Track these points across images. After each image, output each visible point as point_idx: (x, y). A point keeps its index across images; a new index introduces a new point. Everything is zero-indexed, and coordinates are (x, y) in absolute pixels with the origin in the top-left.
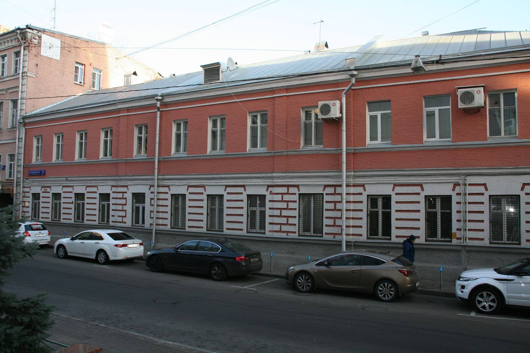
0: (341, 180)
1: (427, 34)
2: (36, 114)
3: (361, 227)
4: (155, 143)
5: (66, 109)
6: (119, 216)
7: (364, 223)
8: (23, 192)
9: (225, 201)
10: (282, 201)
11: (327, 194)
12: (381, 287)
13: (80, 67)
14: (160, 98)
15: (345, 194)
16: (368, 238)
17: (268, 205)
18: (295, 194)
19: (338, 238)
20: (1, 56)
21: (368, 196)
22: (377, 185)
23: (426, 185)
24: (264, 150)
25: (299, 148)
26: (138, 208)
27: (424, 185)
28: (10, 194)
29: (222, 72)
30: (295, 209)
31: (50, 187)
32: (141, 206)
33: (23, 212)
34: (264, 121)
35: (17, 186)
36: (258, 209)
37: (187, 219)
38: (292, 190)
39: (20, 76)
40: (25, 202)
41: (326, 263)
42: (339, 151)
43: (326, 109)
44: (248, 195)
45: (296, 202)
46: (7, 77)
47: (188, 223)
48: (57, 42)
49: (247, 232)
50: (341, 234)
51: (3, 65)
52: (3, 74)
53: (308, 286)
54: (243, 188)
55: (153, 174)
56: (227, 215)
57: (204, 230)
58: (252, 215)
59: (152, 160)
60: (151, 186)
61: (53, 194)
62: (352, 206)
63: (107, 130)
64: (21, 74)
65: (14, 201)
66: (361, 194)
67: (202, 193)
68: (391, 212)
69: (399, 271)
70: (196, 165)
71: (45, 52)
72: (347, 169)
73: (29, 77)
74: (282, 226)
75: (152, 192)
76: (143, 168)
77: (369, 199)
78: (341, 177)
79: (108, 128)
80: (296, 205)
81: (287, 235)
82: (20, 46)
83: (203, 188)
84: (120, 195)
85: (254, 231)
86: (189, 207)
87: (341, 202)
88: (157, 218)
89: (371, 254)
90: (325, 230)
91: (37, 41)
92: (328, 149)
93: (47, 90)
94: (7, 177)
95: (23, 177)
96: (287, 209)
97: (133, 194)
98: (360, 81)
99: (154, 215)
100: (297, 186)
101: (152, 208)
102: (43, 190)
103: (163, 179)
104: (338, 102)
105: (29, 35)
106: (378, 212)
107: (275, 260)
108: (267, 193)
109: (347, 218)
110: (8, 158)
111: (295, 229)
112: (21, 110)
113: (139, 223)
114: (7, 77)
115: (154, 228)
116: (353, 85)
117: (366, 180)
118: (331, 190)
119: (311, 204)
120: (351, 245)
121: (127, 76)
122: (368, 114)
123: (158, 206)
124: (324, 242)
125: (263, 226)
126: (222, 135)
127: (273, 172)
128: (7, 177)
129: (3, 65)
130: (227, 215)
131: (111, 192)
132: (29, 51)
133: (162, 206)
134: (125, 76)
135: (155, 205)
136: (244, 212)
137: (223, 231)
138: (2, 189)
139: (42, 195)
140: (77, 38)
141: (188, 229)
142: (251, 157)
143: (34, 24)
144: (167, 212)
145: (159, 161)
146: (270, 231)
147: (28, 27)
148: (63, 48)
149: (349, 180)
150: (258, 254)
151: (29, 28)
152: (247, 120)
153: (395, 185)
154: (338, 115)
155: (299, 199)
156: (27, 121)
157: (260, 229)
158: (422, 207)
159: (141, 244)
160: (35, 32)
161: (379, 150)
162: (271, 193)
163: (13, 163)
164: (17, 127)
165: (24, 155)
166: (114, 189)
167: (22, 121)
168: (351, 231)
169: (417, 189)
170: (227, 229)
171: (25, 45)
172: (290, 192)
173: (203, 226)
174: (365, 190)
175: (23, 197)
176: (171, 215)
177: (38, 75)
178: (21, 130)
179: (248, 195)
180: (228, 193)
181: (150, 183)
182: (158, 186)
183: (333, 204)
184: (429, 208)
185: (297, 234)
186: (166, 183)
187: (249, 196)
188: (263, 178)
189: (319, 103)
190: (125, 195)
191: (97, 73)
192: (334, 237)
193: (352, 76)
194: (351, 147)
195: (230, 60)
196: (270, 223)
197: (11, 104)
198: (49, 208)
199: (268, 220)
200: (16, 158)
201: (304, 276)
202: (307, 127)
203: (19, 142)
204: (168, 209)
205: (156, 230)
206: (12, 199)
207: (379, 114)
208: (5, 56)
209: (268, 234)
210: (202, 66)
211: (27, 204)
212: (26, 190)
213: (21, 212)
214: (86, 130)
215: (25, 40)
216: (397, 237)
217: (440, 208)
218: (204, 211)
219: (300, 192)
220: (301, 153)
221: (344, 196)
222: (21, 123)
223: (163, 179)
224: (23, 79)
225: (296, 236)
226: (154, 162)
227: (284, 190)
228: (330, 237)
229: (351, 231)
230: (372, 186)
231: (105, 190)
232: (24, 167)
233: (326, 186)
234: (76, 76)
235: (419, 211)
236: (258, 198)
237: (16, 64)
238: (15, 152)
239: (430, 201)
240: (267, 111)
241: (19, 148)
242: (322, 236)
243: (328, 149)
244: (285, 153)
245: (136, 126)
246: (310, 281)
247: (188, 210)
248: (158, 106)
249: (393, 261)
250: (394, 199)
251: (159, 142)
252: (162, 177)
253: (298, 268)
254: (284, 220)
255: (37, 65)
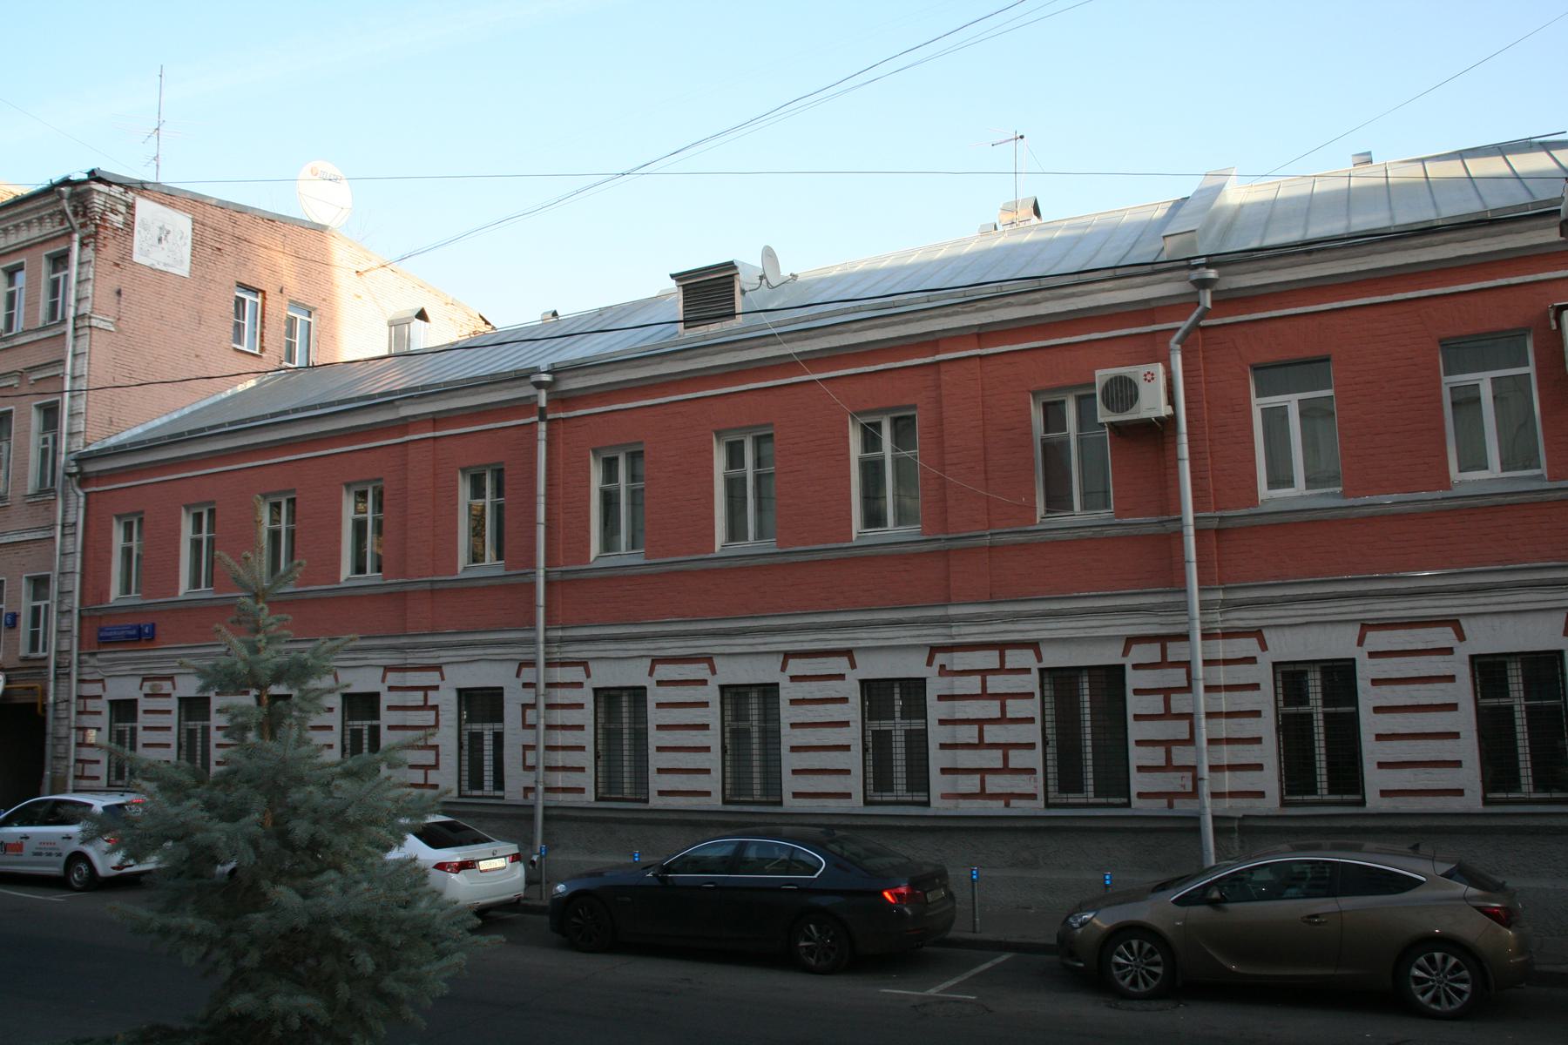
0: (1185, 619)
1: (1366, 159)
2: (124, 446)
3: (1259, 767)
4: (533, 523)
5: (222, 425)
6: (412, 767)
7: (1268, 753)
8: (79, 697)
9: (784, 705)
10: (984, 695)
11: (1136, 667)
12: (1420, 968)
13: (249, 298)
14: (546, 378)
15: (1200, 663)
16: (1284, 804)
17: (936, 710)
18: (1027, 671)
19: (1183, 807)
20: (4, 270)
21: (1275, 664)
22: (1306, 628)
23: (1472, 621)
24: (911, 531)
25: (1033, 522)
26: (477, 738)
27: (1463, 622)
28: (34, 705)
29: (743, 292)
30: (1031, 720)
31: (170, 678)
32: (488, 730)
33: (77, 761)
34: (900, 440)
35: (57, 678)
36: (898, 727)
37: (652, 769)
38: (1015, 658)
39: (70, 327)
40: (85, 729)
41: (1216, 895)
42: (1171, 527)
43: (1123, 393)
44: (863, 682)
45: (1030, 695)
46: (26, 332)
47: (656, 782)
48: (181, 224)
49: (867, 803)
50: (1195, 793)
51: (11, 297)
52: (9, 326)
53: (1154, 975)
54: (844, 661)
55: (532, 625)
56: (794, 749)
57: (715, 802)
58: (878, 747)
59: (526, 580)
60: (524, 664)
61: (181, 700)
62: (1224, 702)
63: (360, 488)
64: (71, 321)
65: (50, 729)
66: (1251, 660)
67: (704, 682)
68: (1357, 713)
69: (1479, 908)
70: (681, 590)
71: (145, 250)
72: (1200, 581)
73: (95, 332)
74: (989, 778)
75: (525, 685)
76: (498, 607)
77: (1279, 677)
78: (1184, 608)
79: (368, 481)
80: (1031, 708)
81: (1007, 805)
82: (68, 235)
83: (706, 665)
84: (416, 698)
85: (888, 797)
86: (660, 727)
87: (1188, 689)
88: (548, 768)
89: (1337, 853)
90: (1138, 782)
91: (120, 218)
92: (1131, 520)
93: (147, 375)
94: (24, 651)
95: (80, 648)
96: (1003, 720)
97: (460, 691)
98: (1228, 301)
99: (538, 758)
100: (1034, 645)
101: (528, 737)
102: (147, 688)
103: (564, 641)
104: (1159, 369)
105: (98, 201)
106: (1510, 709)
107: (986, 890)
108: (930, 673)
109: (1211, 741)
110: (25, 588)
111: (1034, 785)
112: (71, 434)
113: (481, 787)
114: (26, 332)
115: (540, 800)
116: (1206, 314)
117: (1265, 614)
118: (1150, 653)
119: (750, 707)
120: (1232, 830)
121: (397, 325)
122: (1257, 405)
123: (549, 727)
124: (1136, 824)
125: (919, 779)
126: (633, 504)
127: (948, 602)
128: (24, 651)
129: (11, 297)
130: (794, 749)
131: (381, 688)
132: (96, 250)
133: (564, 727)
134: (392, 324)
135: (542, 727)
136: (852, 736)
137: (780, 803)
138: (5, 690)
139: (143, 704)
140: (241, 210)
141: (656, 802)
142: (868, 559)
143: (108, 167)
144: (582, 748)
145: (548, 583)
146: (945, 796)
147: (94, 176)
148: (197, 243)
149: (1209, 618)
150: (937, 877)
151: (100, 180)
152: (847, 437)
153: (1366, 626)
154: (1164, 410)
155: (1042, 686)
156: (90, 468)
157: (910, 788)
158: (1463, 691)
159: (515, 858)
160: (116, 190)
161: (1305, 517)
162: (943, 671)
163: (42, 603)
164: (58, 486)
165: (83, 576)
166: (393, 679)
167: (75, 470)
168: (1228, 782)
169: (1444, 637)
170: (796, 795)
171: (86, 231)
172: (1008, 666)
173: (711, 790)
174: (714, 672)
175: (79, 713)
176: (597, 757)
177: (122, 324)
178: (72, 498)
179: (863, 682)
180: (793, 678)
181: (520, 653)
182: (549, 664)
183: (1161, 697)
184: (1483, 697)
185: (1040, 803)
186: (573, 652)
187: (868, 687)
188: (913, 623)
189: (1098, 373)
190: (433, 698)
191: (301, 317)
192: (1170, 806)
193: (1203, 284)
194: (1208, 510)
195: (769, 254)
196: (944, 771)
197: (36, 420)
198: (168, 746)
199: (937, 759)
200: (54, 587)
201: (1135, 944)
202: (1055, 454)
203: (63, 535)
204: (587, 738)
205: (545, 808)
206: (43, 721)
207: (1292, 402)
208: (20, 267)
209: (938, 806)
210: (672, 276)
211: (92, 736)
212: (89, 689)
213: (72, 762)
214: (293, 491)
215: (85, 215)
216: (1384, 793)
217: (1320, 703)
218: (713, 738)
219: (1044, 665)
220: (1038, 537)
221: (1199, 670)
222: (70, 475)
223: (564, 641)
224: (76, 337)
225: (1037, 807)
226: (532, 586)
227: (989, 659)
228: (1157, 807)
229: (1228, 782)
230: (1287, 631)
231: (364, 681)
232: (81, 618)
233: (1130, 641)
234: (238, 328)
235: (1453, 707)
236: (897, 690)
237: (55, 293)
238: (51, 569)
239: (1291, 677)
240: (914, 407)
241: (63, 554)
242: (1128, 805)
243: (1131, 520)
244: (986, 541)
245: (464, 470)
246: (1158, 957)
247: (655, 738)
248: (543, 403)
249: (1448, 875)
250: (1366, 670)
251: (548, 519)
252: (560, 633)
253: (1100, 920)
254: (993, 759)
255: (119, 293)
